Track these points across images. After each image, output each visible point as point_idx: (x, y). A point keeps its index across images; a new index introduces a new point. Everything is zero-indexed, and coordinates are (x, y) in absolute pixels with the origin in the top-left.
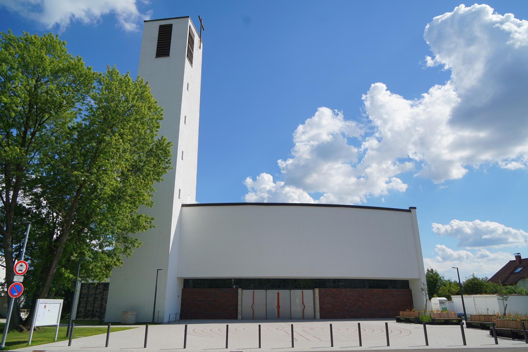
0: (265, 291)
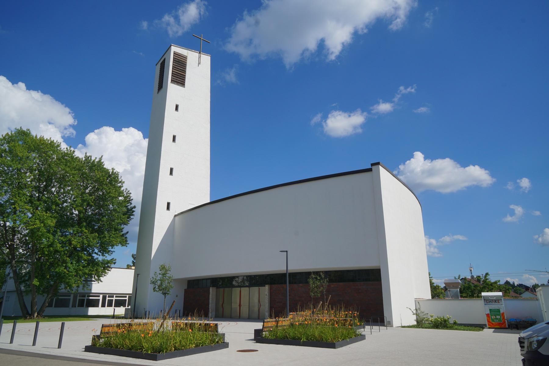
0: (249, 289)
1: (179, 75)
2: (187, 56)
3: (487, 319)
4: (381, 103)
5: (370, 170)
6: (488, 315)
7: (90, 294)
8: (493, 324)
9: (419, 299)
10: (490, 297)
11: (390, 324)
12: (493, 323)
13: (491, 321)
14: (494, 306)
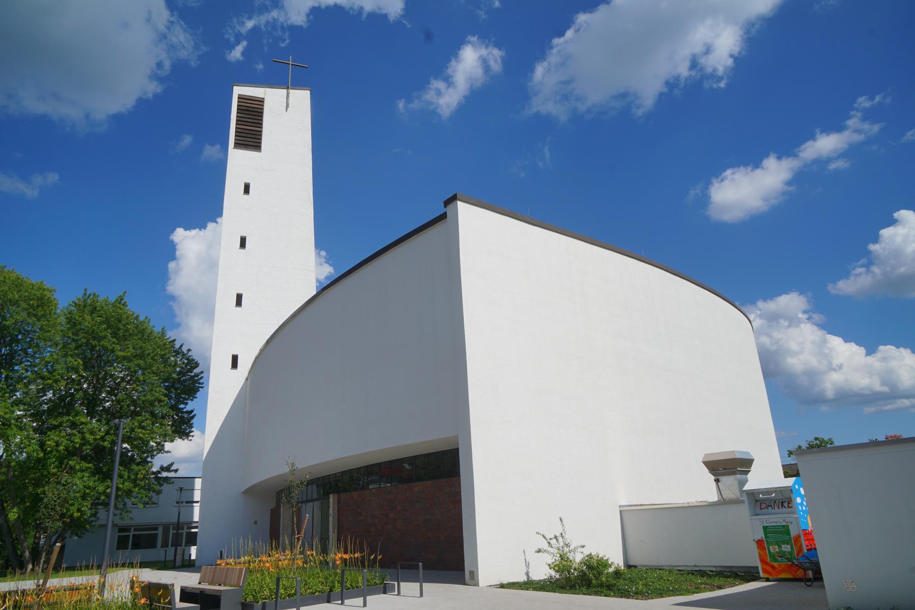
1: (246, 131)
2: (264, 99)
3: (760, 556)
4: (818, 136)
5: (443, 217)
6: (760, 543)
7: (191, 524)
8: (773, 567)
9: (641, 505)
10: (759, 493)
11: (473, 580)
12: (776, 564)
13: (769, 561)
14: (775, 518)
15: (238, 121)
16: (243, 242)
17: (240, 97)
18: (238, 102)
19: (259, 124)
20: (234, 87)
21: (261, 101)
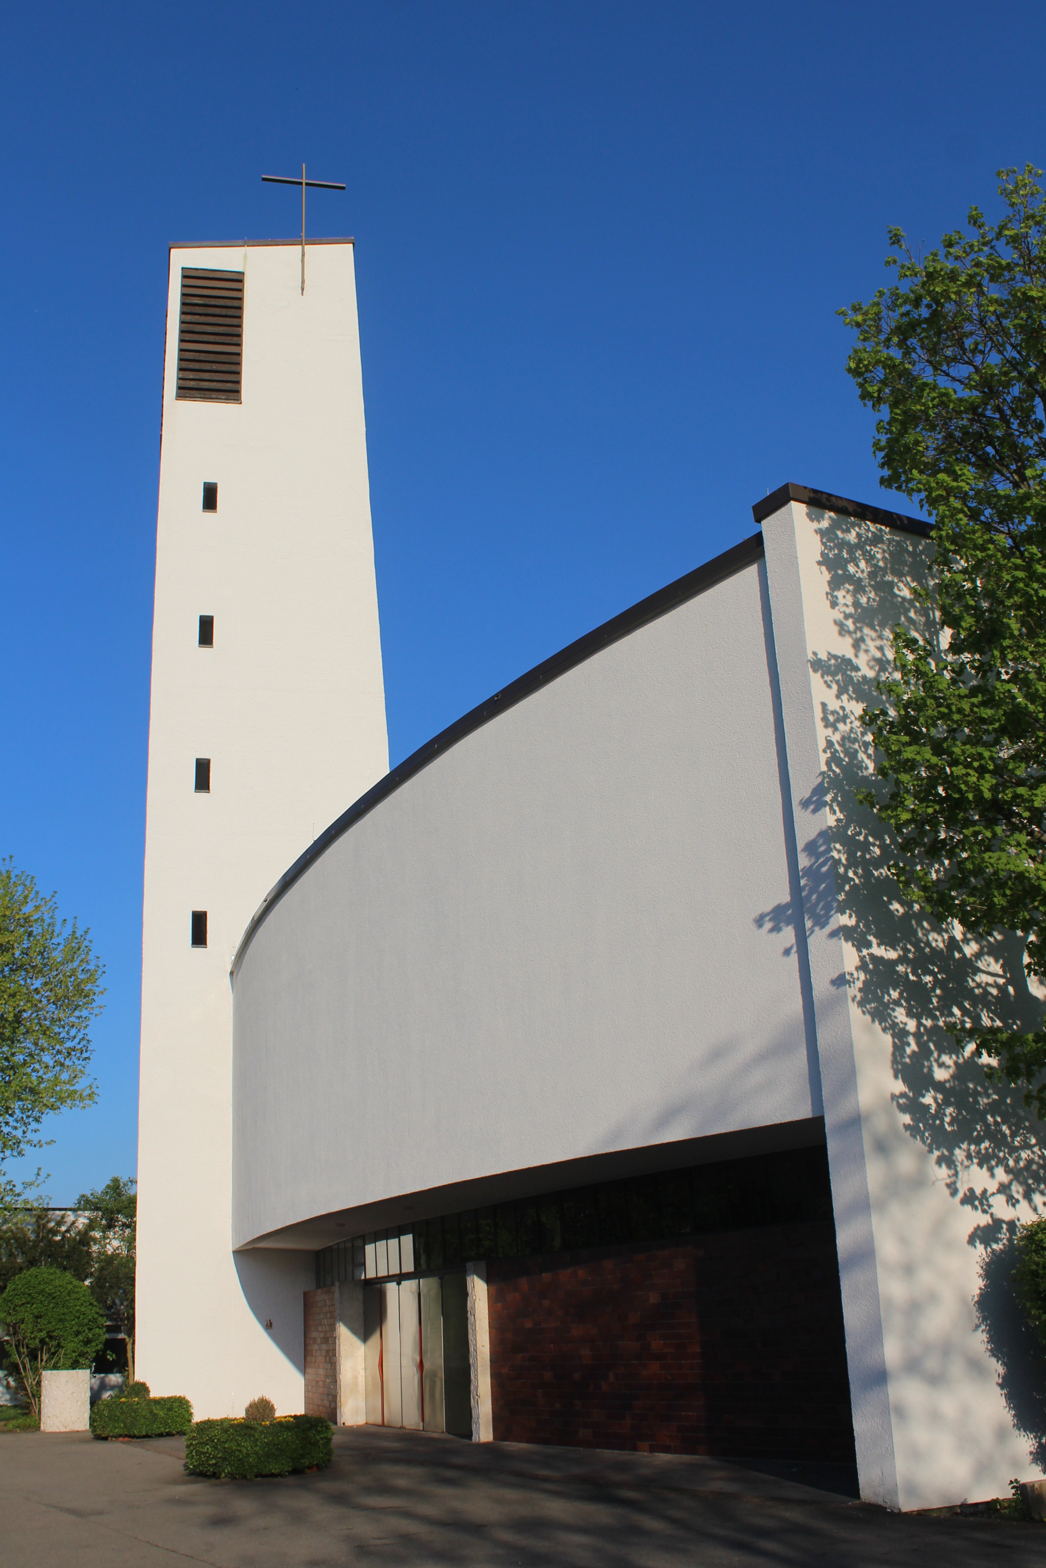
1: (202, 356)
2: (242, 273)
15: (186, 333)
16: (210, 498)
17: (188, 275)
18: (183, 286)
19: (235, 336)
20: (172, 250)
21: (237, 279)
